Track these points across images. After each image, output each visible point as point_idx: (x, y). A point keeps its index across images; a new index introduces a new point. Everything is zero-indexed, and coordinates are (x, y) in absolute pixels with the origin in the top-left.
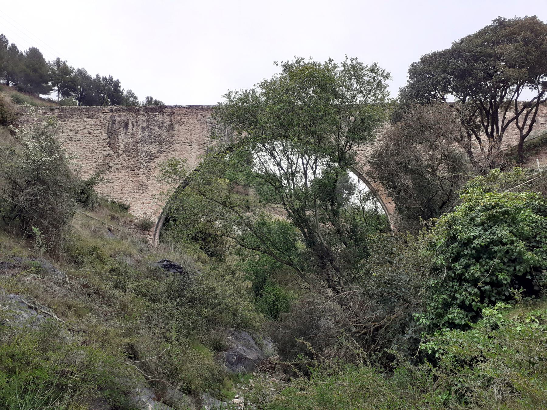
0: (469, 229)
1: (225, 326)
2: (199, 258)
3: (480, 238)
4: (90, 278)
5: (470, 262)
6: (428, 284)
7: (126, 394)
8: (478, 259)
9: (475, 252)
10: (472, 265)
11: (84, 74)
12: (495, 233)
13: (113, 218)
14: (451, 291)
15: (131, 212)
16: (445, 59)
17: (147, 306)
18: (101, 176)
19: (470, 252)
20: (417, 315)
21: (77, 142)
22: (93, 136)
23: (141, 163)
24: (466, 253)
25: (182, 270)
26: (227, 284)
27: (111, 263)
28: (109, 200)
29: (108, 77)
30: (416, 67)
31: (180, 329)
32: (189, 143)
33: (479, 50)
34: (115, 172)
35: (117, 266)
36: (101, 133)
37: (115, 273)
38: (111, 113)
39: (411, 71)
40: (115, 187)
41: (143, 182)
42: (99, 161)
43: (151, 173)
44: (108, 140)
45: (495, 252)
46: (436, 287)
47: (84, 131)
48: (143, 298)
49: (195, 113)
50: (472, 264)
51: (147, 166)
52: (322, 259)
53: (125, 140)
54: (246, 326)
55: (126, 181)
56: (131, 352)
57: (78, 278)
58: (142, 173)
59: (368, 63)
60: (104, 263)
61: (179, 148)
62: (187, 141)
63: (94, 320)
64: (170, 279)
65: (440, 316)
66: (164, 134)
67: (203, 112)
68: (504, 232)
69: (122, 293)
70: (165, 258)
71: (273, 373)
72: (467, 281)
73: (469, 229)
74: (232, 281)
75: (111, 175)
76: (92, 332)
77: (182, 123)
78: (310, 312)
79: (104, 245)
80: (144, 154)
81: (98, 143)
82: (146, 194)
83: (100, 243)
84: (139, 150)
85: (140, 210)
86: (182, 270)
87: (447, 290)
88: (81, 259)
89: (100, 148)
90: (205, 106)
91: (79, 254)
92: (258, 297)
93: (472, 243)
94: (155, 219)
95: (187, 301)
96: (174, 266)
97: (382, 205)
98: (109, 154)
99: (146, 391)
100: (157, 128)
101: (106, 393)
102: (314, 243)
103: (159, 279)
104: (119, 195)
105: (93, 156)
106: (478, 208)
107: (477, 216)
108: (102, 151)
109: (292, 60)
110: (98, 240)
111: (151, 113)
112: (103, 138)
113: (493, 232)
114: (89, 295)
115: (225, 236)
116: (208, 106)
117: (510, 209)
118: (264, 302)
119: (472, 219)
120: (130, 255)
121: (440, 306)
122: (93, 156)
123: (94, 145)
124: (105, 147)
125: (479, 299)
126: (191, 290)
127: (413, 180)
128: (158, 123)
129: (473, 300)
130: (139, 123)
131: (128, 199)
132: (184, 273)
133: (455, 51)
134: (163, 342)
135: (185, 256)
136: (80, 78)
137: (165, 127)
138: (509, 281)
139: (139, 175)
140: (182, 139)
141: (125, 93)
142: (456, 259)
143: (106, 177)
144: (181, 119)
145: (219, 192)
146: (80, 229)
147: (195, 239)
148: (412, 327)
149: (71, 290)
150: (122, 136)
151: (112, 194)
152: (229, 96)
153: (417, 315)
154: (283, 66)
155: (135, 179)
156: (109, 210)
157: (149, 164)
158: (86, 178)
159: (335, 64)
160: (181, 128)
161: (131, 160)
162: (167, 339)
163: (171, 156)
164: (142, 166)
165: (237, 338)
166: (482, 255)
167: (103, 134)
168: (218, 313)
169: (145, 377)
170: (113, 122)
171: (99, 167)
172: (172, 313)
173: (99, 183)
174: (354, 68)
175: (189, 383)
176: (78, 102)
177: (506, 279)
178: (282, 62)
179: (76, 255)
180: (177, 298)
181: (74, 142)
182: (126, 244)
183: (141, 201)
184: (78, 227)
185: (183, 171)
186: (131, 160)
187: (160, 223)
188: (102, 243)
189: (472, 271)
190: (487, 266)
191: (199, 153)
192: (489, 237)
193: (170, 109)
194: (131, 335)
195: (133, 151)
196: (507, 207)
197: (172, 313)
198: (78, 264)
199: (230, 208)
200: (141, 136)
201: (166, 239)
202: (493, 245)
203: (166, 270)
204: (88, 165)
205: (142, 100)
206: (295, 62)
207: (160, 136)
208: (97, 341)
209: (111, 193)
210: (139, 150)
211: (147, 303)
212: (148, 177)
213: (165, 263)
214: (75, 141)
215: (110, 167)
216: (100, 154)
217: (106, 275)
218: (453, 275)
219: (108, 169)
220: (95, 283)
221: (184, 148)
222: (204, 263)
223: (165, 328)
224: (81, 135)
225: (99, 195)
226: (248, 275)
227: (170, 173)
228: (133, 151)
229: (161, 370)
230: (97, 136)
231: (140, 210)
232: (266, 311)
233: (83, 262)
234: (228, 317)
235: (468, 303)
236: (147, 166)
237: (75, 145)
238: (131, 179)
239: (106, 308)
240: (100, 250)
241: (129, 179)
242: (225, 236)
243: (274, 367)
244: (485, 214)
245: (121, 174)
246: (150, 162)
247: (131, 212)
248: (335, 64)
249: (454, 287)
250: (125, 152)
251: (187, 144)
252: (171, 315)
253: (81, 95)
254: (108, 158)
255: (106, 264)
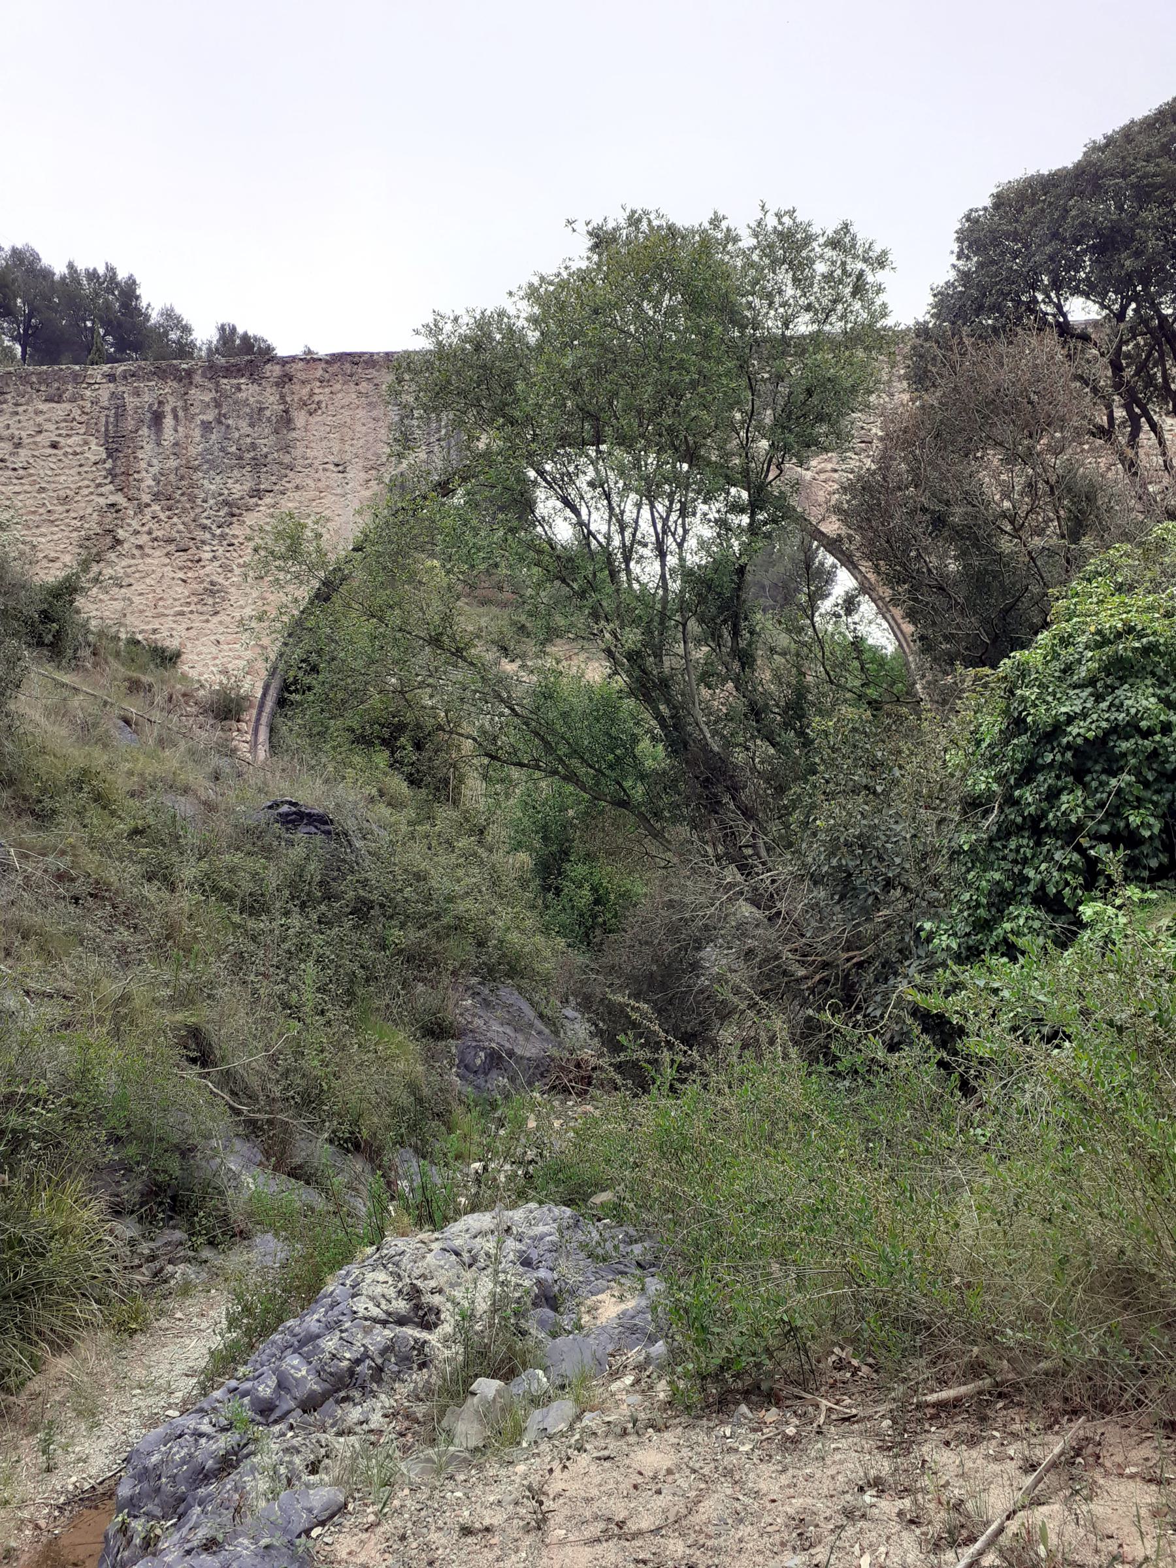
0: (1058, 695)
1: (454, 973)
2: (381, 793)
3: (1085, 720)
4: (75, 855)
5: (1059, 783)
6: (953, 844)
7: (186, 1152)
8: (1079, 775)
9: (1073, 756)
10: (1065, 793)
11: (31, 263)
12: (1122, 704)
13: (135, 686)
14: (1015, 862)
15: (185, 668)
16: (1058, 197)
17: (237, 926)
18: (95, 568)
19: (1059, 757)
20: (928, 926)
21: (21, 472)
22: (66, 454)
23: (204, 527)
24: (1049, 761)
25: (331, 827)
26: (462, 860)
27: (135, 812)
28: (123, 636)
29: (101, 271)
30: (977, 221)
31: (327, 985)
32: (337, 465)
33: (1151, 169)
34: (133, 557)
35: (151, 820)
36: (86, 443)
37: (144, 841)
38: (111, 385)
39: (962, 237)
40: (136, 599)
41: (212, 583)
42: (86, 526)
43: (235, 554)
44: (108, 465)
45: (1124, 755)
46: (973, 850)
47: (38, 439)
48: (224, 904)
49: (351, 376)
50: (1065, 788)
51: (223, 536)
52: (706, 787)
53: (155, 462)
54: (513, 972)
55: (166, 581)
56: (193, 1046)
57: (44, 855)
58: (209, 555)
59: (824, 223)
60: (113, 813)
61: (310, 482)
62: (331, 458)
63: (93, 966)
64: (297, 853)
65: (984, 926)
66: (266, 442)
67: (373, 373)
68: (1144, 703)
69: (166, 894)
70: (283, 796)
71: (586, 1092)
72: (1054, 833)
73: (1058, 695)
74: (475, 854)
75: (124, 563)
76: (86, 996)
77: (314, 406)
78: (673, 930)
79: (110, 765)
80: (212, 502)
81: (79, 473)
82: (225, 617)
83: (100, 758)
84: (196, 491)
85: (211, 663)
86: (331, 827)
87: (1004, 858)
88: (48, 803)
89: (88, 487)
90: (378, 354)
91: (43, 791)
92: (550, 895)
93: (1065, 733)
94: (253, 686)
95: (349, 910)
96: (309, 815)
97: (892, 628)
98: (113, 505)
99: (238, 1144)
100: (244, 424)
101: (132, 1150)
102: (686, 745)
103: (268, 852)
104: (149, 623)
105: (68, 511)
106: (1083, 639)
107: (1079, 661)
108: (92, 497)
109: (616, 218)
110: (97, 751)
111: (225, 381)
112: (93, 459)
113: (1117, 702)
114: (76, 900)
115: (444, 730)
116: (387, 354)
117: (1162, 641)
118: (568, 906)
119: (1068, 669)
120: (186, 790)
121: (984, 901)
122: (68, 511)
123: (68, 479)
124: (99, 485)
125: (1081, 880)
126: (358, 881)
127: (962, 555)
128: (248, 410)
129: (1067, 884)
130: (193, 410)
131: (174, 633)
132: (337, 834)
133: (1084, 172)
134: (278, 1016)
135: (340, 789)
136: (18, 274)
137: (269, 420)
138: (1156, 831)
139: (202, 563)
140: (317, 453)
141: (155, 317)
142: (1028, 773)
143: (107, 572)
144: (312, 394)
145: (421, 609)
146: (43, 721)
147: (362, 740)
148: (919, 957)
149: (24, 890)
150: (147, 451)
151: (130, 619)
152: (433, 330)
153: (928, 926)
154: (590, 234)
155: (190, 575)
156: (123, 664)
157: (227, 530)
158: (51, 575)
159: (728, 230)
160: (313, 420)
161: (175, 520)
162: (293, 1010)
163: (290, 505)
164: (208, 536)
165: (486, 1004)
166: (1089, 764)
167: (94, 447)
168: (434, 941)
169: (231, 1107)
170: (120, 411)
171: (87, 543)
172: (306, 942)
173: (89, 589)
174: (786, 236)
175: (355, 1122)
176: (18, 349)
177: (1150, 827)
178: (587, 224)
179: (35, 793)
180: (320, 903)
181: (11, 473)
182: (172, 759)
183: (213, 638)
184: (37, 715)
185: (319, 550)
186: (175, 520)
187: (269, 698)
188: (106, 758)
189: (1063, 808)
190: (1102, 792)
191: (368, 493)
192: (1107, 716)
193: (277, 368)
194: (192, 1002)
195: (182, 494)
196: (1154, 633)
197: (306, 942)
198: (43, 818)
199: (453, 654)
200: (200, 448)
201: (292, 741)
202: (1119, 738)
203: (287, 829)
204: (55, 537)
205: (204, 334)
206: (623, 223)
207: (254, 446)
208: (101, 1020)
209: (125, 615)
210: (196, 491)
211: (236, 918)
212: (227, 569)
213: (285, 808)
214: (14, 469)
215: (118, 542)
216: (90, 505)
217: (120, 847)
218: (1019, 820)
219: (112, 547)
220: (90, 868)
221: (323, 479)
222: (395, 804)
223: (284, 981)
224: (29, 453)
225: (93, 623)
226: (520, 837)
227: (282, 557)
228: (182, 494)
229: (277, 1092)
230: (75, 454)
231: (211, 663)
232: (572, 931)
233: (54, 811)
234: (463, 950)
235: (1054, 891)
236: (223, 536)
237: (15, 481)
238: (181, 575)
239: (123, 935)
240: (100, 777)
241: (172, 575)
242: (444, 730)
243: (590, 1077)
244: (1097, 654)
245: (148, 560)
246: (231, 524)
247: (185, 668)
248: (728, 230)
249: (1022, 850)
250: (156, 497)
251: (331, 467)
252: (303, 948)
253: (28, 326)
254: (110, 516)
255: (119, 817)
